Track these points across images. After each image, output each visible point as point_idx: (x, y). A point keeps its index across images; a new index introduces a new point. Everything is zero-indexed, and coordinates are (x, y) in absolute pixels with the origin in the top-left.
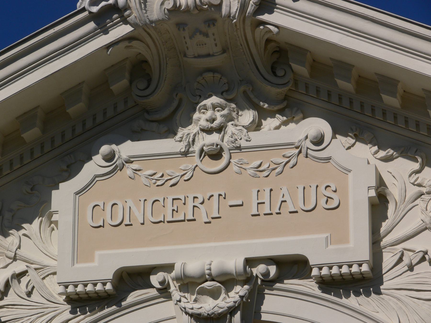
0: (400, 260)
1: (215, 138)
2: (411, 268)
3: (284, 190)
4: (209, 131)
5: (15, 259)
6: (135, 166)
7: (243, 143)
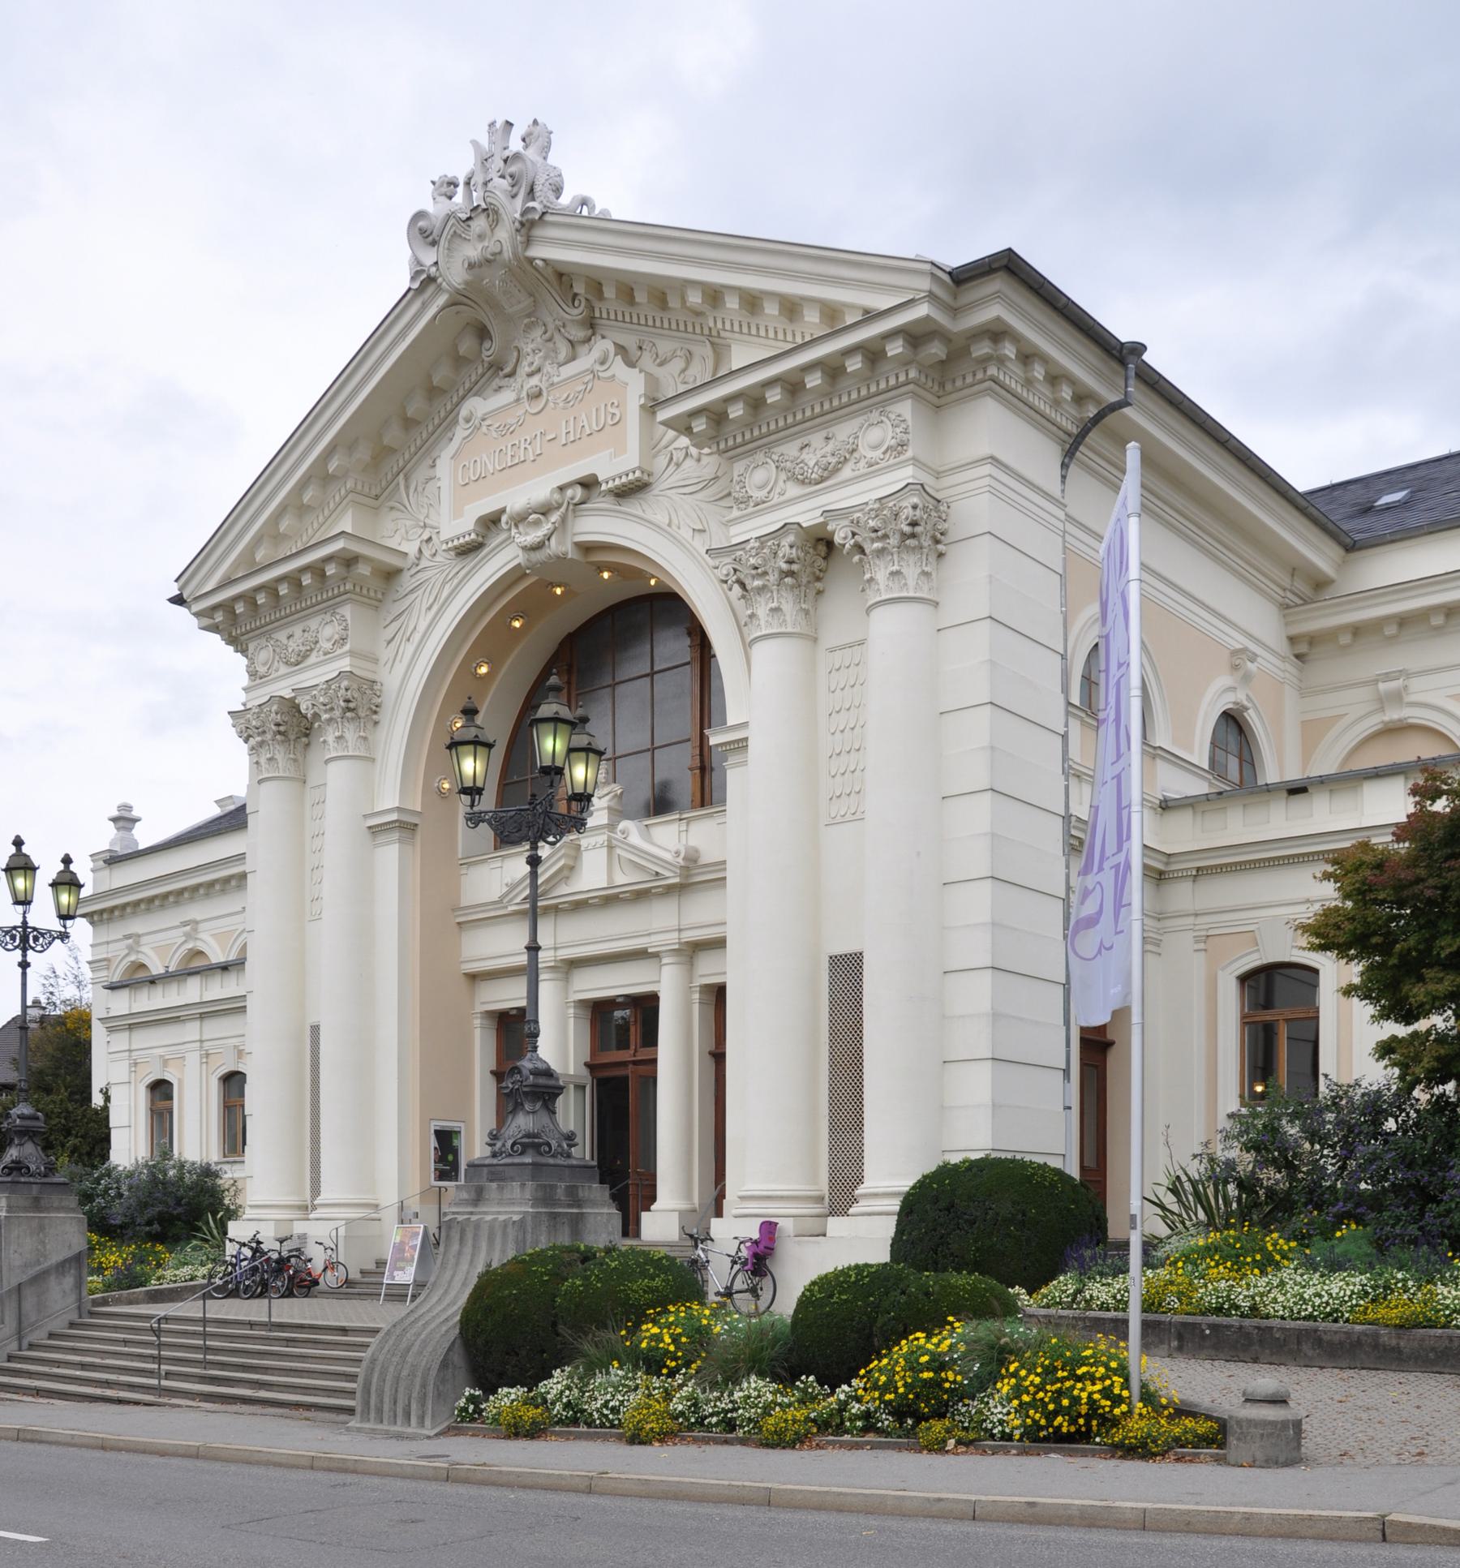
0: (671, 459)
1: (535, 381)
2: (678, 465)
3: (584, 416)
4: (530, 375)
5: (425, 526)
6: (488, 422)
7: (556, 380)
